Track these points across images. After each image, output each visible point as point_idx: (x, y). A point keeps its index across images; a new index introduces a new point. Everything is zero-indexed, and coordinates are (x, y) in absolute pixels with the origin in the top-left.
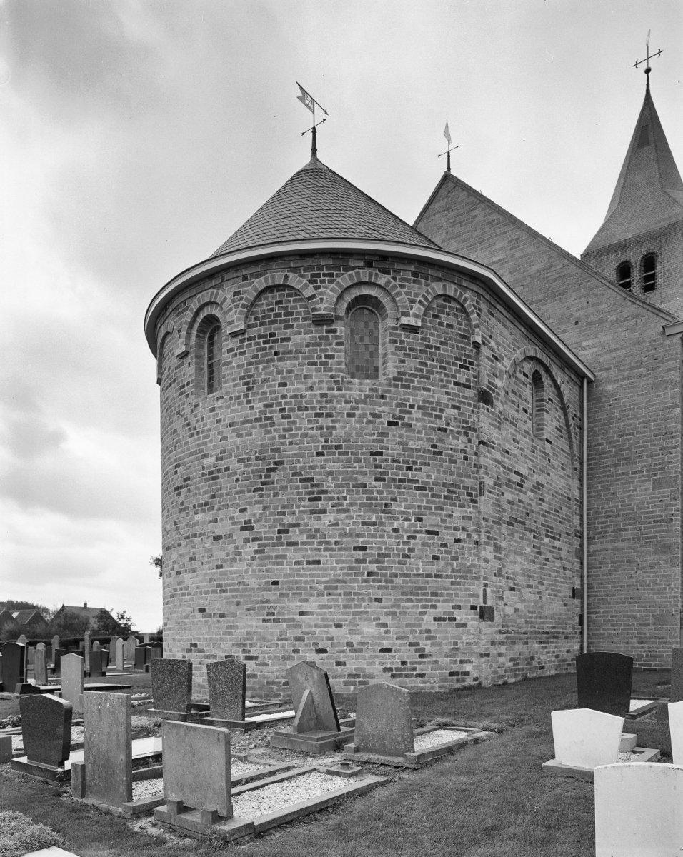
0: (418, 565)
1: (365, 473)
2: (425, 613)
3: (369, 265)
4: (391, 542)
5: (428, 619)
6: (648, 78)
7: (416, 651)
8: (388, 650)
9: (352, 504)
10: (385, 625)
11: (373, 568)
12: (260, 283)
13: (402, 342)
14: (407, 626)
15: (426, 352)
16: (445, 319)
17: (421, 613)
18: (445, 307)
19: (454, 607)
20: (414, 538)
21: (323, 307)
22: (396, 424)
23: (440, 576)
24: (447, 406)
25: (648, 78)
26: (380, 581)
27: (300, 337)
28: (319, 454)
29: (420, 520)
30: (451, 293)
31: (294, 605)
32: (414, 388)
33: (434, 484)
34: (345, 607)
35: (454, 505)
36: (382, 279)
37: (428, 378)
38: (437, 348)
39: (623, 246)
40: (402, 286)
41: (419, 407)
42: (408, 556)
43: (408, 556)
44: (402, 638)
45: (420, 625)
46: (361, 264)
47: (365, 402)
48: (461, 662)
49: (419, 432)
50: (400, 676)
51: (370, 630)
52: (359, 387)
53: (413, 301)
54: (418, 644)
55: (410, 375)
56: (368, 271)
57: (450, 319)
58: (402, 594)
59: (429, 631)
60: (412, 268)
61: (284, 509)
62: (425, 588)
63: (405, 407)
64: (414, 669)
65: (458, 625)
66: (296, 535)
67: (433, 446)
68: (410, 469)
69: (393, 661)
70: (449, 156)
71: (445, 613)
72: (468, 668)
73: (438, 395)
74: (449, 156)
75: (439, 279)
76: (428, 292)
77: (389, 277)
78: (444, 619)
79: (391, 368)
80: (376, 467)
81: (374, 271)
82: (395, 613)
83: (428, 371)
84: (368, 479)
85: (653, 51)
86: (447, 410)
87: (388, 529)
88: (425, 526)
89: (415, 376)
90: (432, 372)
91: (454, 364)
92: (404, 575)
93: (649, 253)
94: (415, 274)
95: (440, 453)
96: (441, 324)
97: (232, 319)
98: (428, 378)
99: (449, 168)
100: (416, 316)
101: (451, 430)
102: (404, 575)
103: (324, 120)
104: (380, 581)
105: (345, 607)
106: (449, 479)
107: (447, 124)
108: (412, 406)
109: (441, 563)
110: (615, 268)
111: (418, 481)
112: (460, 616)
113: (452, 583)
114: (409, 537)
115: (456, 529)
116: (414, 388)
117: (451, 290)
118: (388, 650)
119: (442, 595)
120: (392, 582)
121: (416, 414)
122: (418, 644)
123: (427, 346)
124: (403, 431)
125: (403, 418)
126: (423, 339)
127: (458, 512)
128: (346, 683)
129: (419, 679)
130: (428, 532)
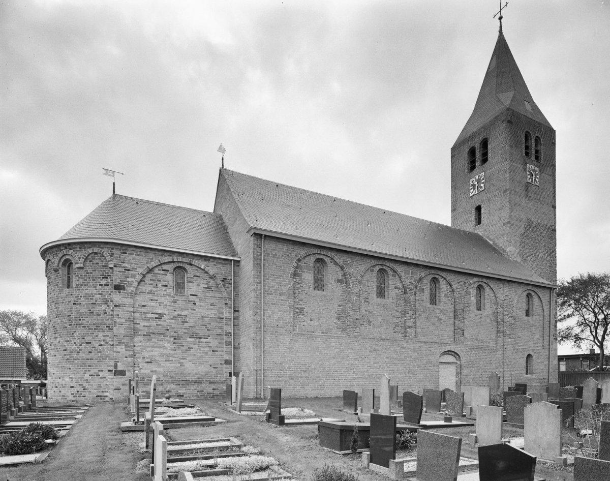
0: (83, 355)
1: (66, 323)
2: (86, 373)
3: (66, 248)
4: (73, 347)
5: (87, 376)
6: (501, 22)
8: (72, 387)
9: (63, 335)
10: (71, 378)
11: (68, 357)
13: (78, 273)
14: (79, 378)
15: (86, 275)
16: (95, 261)
17: (84, 373)
18: (95, 257)
20: (81, 345)
22: (75, 304)
23: (93, 359)
24: (96, 294)
25: (501, 22)
26: (70, 362)
28: (56, 317)
29: (84, 338)
30: (96, 251)
32: (82, 290)
33: (90, 324)
34: (62, 371)
35: (99, 332)
36: (70, 252)
37: (87, 285)
38: (92, 273)
40: (76, 253)
42: (79, 352)
43: (79, 352)
44: (77, 382)
45: (83, 378)
46: (64, 248)
47: (66, 297)
48: (103, 392)
49: (84, 306)
50: (76, 396)
51: (67, 379)
53: (80, 258)
54: (83, 385)
55: (80, 285)
57: (98, 261)
58: (77, 366)
59: (87, 380)
60: (79, 246)
62: (86, 364)
63: (79, 297)
64: (81, 394)
68: (80, 320)
69: (74, 391)
71: (94, 373)
72: (106, 394)
75: (90, 247)
76: (85, 253)
78: (94, 375)
80: (69, 320)
82: (75, 373)
83: (88, 283)
84: (67, 325)
85: (503, 4)
86: (96, 296)
87: (73, 342)
89: (83, 285)
90: (89, 283)
91: (99, 278)
92: (78, 359)
93: (484, 139)
94: (80, 248)
96: (93, 264)
98: (87, 285)
100: (81, 263)
101: (98, 303)
102: (78, 359)
104: (70, 362)
105: (62, 371)
106: (96, 322)
107: (502, 52)
108: (81, 297)
109: (93, 354)
110: (467, 152)
111: (83, 324)
112: (101, 374)
113: (98, 362)
114: (80, 345)
115: (99, 341)
116: (82, 290)
117: (96, 250)
118: (72, 387)
119: (93, 366)
120: (74, 362)
121: (82, 299)
122: (83, 385)
123: (87, 273)
124: (78, 306)
125: (78, 301)
126: (85, 271)
127: (101, 334)
128: (62, 399)
129: (83, 398)
130: (87, 343)
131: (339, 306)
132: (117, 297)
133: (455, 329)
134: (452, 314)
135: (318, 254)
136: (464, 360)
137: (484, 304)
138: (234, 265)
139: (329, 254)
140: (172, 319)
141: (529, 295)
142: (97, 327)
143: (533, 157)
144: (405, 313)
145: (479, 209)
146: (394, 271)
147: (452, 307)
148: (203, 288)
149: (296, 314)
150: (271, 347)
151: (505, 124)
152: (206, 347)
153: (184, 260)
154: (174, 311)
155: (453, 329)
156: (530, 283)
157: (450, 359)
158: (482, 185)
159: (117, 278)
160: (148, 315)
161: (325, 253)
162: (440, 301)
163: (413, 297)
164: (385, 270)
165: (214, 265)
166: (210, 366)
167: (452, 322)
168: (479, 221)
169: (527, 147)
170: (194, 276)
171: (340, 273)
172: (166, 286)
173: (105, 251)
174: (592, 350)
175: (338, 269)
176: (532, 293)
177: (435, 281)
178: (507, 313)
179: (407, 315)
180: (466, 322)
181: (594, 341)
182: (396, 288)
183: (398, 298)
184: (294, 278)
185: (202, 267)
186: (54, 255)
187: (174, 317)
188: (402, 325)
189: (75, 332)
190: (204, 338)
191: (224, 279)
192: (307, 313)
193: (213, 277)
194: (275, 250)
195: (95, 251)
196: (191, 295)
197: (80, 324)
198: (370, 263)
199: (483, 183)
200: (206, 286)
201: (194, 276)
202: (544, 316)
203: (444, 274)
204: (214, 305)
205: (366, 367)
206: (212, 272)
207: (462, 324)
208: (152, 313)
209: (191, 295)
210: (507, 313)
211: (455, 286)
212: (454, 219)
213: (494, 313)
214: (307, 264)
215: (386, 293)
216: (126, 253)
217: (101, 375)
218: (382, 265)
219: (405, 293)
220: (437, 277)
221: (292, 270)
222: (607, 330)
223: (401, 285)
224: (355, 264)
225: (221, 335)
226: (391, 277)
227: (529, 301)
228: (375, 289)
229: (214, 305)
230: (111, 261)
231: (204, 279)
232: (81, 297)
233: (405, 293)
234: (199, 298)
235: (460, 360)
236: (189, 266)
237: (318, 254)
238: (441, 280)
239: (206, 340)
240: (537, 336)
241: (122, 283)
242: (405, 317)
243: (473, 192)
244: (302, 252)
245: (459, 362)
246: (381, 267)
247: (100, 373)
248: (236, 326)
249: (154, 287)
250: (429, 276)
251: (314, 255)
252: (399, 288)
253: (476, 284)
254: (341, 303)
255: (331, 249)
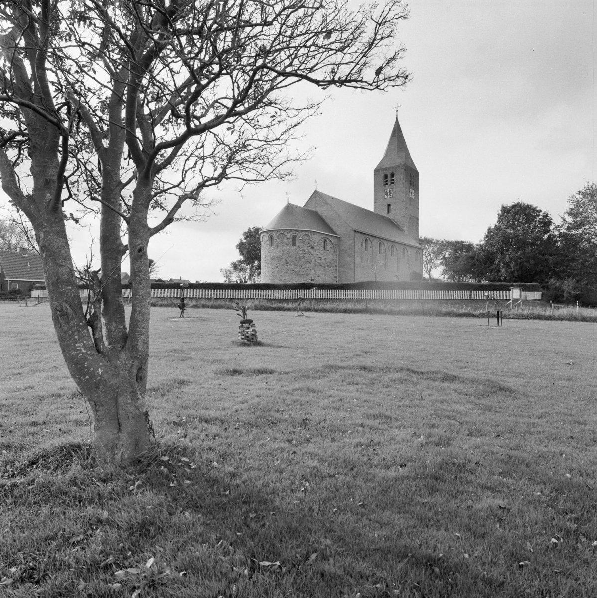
12: (279, 233)
21: (288, 237)
27: (285, 241)
31: (284, 278)
39: (385, 169)
52: (293, 248)
61: (283, 265)
66: (284, 268)
73: (305, 248)
79: (298, 245)
97: (275, 237)
107: (397, 132)
132: (312, 251)
141: (366, 240)
142: (306, 262)
145: (389, 205)
151: (403, 170)
168: (389, 212)
169: (410, 181)
212: (374, 210)
222: (37, 239)
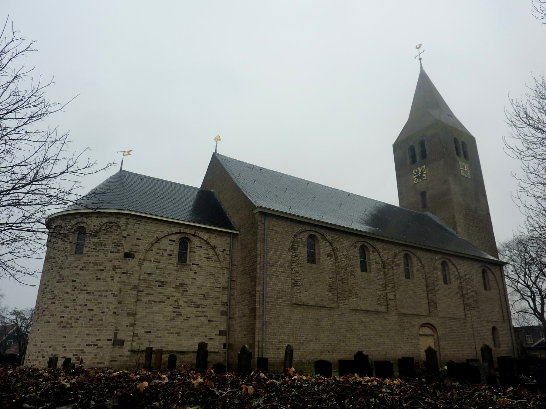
3: (82, 216)
6: (421, 62)
7: (76, 358)
19: (97, 340)
22: (82, 270)
25: (421, 62)
36: (85, 220)
41: (93, 263)
46: (79, 216)
54: (77, 355)
56: (81, 218)
59: (83, 350)
60: (96, 215)
65: (98, 348)
67: (97, 276)
70: (216, 146)
71: (92, 342)
74: (216, 146)
75: (107, 217)
77: (88, 219)
81: (83, 218)
88: (88, 307)
94: (97, 217)
95: (99, 279)
99: (216, 151)
103: (117, 152)
108: (90, 263)
111: (87, 290)
112: (100, 344)
121: (91, 265)
131: (330, 278)
133: (429, 302)
134: (425, 288)
135: (311, 230)
136: (440, 332)
137: (450, 279)
138: (233, 237)
139: (320, 231)
140: (173, 288)
141: (484, 272)
143: (463, 156)
144: (386, 286)
146: (374, 248)
147: (424, 281)
148: (205, 258)
149: (293, 285)
150: (272, 318)
152: (203, 317)
153: (187, 231)
154: (176, 279)
155: (427, 302)
156: (447, 252)
157: (428, 331)
158: (424, 175)
159: (127, 247)
160: (152, 283)
161: (317, 230)
162: (413, 275)
163: (391, 271)
164: (314, 236)
165: (216, 237)
166: (206, 337)
167: (425, 294)
170: (197, 246)
171: (329, 248)
172: (171, 255)
173: (122, 221)
174: (539, 324)
175: (328, 244)
176: (486, 269)
177: (407, 257)
178: (470, 287)
179: (388, 288)
180: (437, 295)
181: (535, 314)
182: (376, 263)
183: (379, 272)
184: (291, 252)
185: (205, 239)
186: (67, 222)
187: (176, 286)
188: (384, 298)
189: (77, 298)
190: (202, 308)
191: (223, 250)
192: (302, 284)
193: (213, 248)
194: (275, 226)
195: (111, 221)
196: (193, 264)
197: (84, 290)
198: (354, 239)
199: (425, 174)
200: (207, 256)
201: (197, 246)
202: (499, 290)
203: (414, 251)
204: (213, 275)
205: (356, 339)
206: (213, 242)
207: (434, 297)
208: (156, 281)
209: (193, 264)
210: (470, 287)
211: (424, 262)
213: (458, 287)
214: (302, 239)
215: (368, 267)
216: (139, 224)
217: (99, 345)
218: (363, 241)
219: (384, 267)
220: (409, 253)
221: (290, 245)
223: (380, 260)
224: (342, 240)
225: (217, 304)
226: (371, 253)
227: (408, 262)
228: (359, 263)
229: (213, 275)
230: (125, 230)
231: (205, 250)
232: (90, 263)
233: (384, 267)
234: (200, 267)
235: (437, 333)
236: (193, 238)
237: (311, 230)
238: (412, 256)
239: (203, 310)
240: (497, 310)
241: (132, 251)
242: (387, 290)
243: (416, 180)
244: (298, 228)
245: (436, 335)
246: (362, 243)
247: (98, 342)
248: (232, 295)
249: (161, 256)
250: (403, 252)
251: (308, 232)
252: (379, 263)
253: (441, 261)
254: (331, 276)
255: (327, 228)
